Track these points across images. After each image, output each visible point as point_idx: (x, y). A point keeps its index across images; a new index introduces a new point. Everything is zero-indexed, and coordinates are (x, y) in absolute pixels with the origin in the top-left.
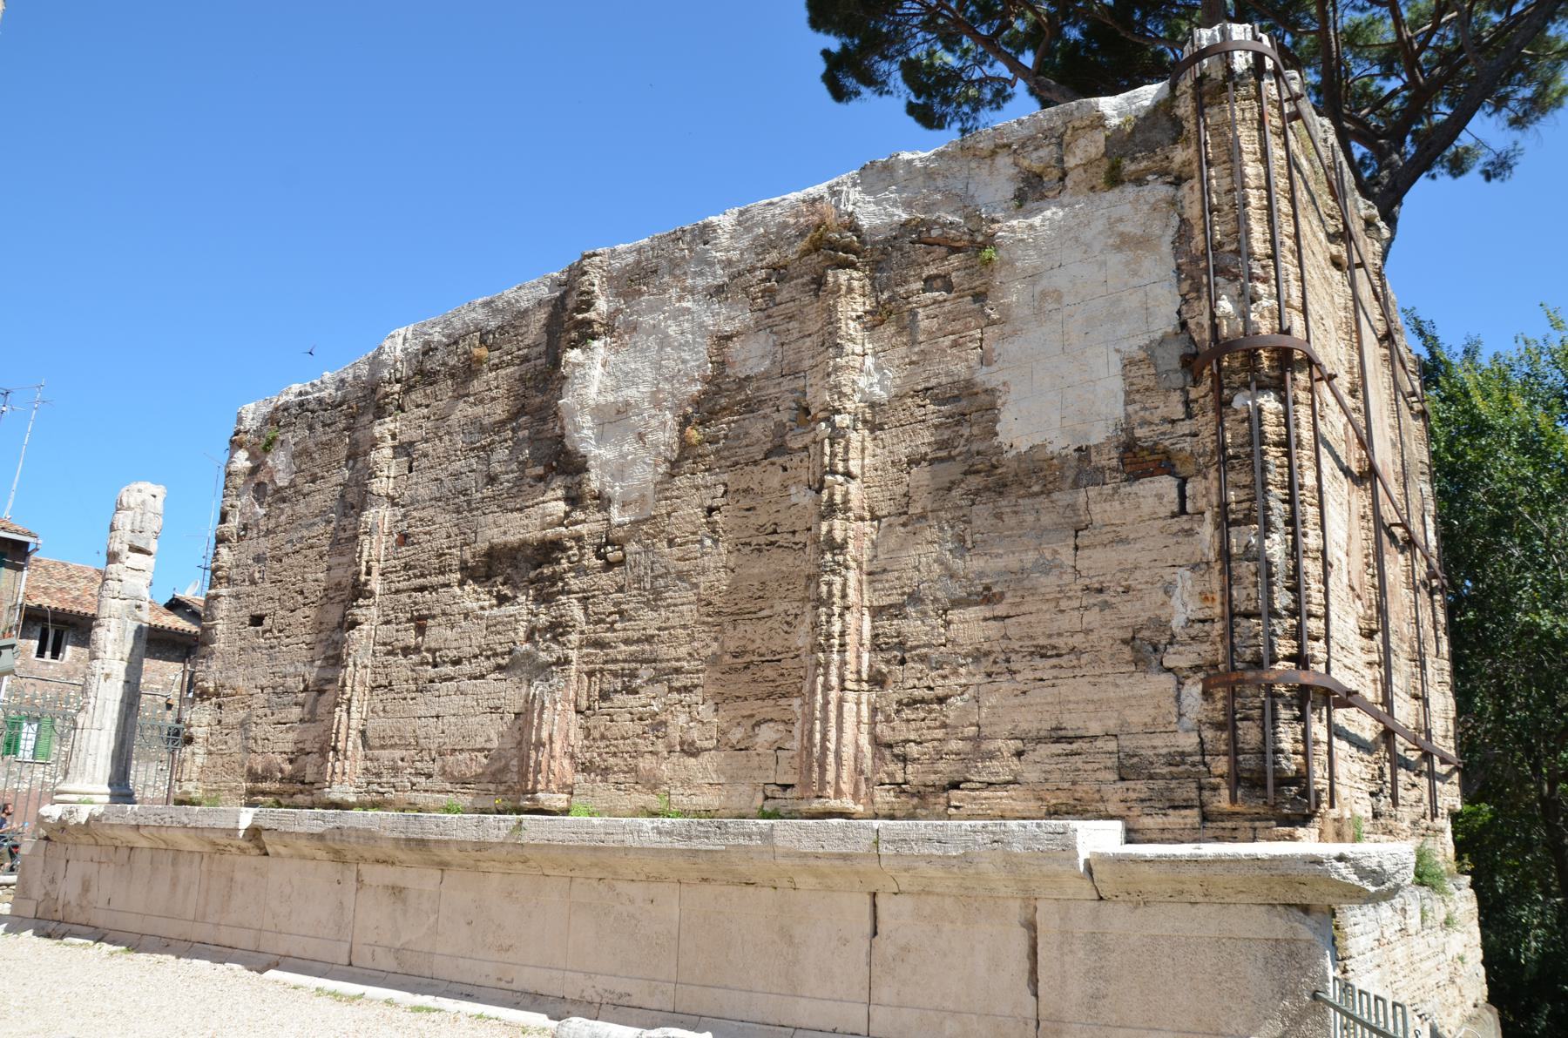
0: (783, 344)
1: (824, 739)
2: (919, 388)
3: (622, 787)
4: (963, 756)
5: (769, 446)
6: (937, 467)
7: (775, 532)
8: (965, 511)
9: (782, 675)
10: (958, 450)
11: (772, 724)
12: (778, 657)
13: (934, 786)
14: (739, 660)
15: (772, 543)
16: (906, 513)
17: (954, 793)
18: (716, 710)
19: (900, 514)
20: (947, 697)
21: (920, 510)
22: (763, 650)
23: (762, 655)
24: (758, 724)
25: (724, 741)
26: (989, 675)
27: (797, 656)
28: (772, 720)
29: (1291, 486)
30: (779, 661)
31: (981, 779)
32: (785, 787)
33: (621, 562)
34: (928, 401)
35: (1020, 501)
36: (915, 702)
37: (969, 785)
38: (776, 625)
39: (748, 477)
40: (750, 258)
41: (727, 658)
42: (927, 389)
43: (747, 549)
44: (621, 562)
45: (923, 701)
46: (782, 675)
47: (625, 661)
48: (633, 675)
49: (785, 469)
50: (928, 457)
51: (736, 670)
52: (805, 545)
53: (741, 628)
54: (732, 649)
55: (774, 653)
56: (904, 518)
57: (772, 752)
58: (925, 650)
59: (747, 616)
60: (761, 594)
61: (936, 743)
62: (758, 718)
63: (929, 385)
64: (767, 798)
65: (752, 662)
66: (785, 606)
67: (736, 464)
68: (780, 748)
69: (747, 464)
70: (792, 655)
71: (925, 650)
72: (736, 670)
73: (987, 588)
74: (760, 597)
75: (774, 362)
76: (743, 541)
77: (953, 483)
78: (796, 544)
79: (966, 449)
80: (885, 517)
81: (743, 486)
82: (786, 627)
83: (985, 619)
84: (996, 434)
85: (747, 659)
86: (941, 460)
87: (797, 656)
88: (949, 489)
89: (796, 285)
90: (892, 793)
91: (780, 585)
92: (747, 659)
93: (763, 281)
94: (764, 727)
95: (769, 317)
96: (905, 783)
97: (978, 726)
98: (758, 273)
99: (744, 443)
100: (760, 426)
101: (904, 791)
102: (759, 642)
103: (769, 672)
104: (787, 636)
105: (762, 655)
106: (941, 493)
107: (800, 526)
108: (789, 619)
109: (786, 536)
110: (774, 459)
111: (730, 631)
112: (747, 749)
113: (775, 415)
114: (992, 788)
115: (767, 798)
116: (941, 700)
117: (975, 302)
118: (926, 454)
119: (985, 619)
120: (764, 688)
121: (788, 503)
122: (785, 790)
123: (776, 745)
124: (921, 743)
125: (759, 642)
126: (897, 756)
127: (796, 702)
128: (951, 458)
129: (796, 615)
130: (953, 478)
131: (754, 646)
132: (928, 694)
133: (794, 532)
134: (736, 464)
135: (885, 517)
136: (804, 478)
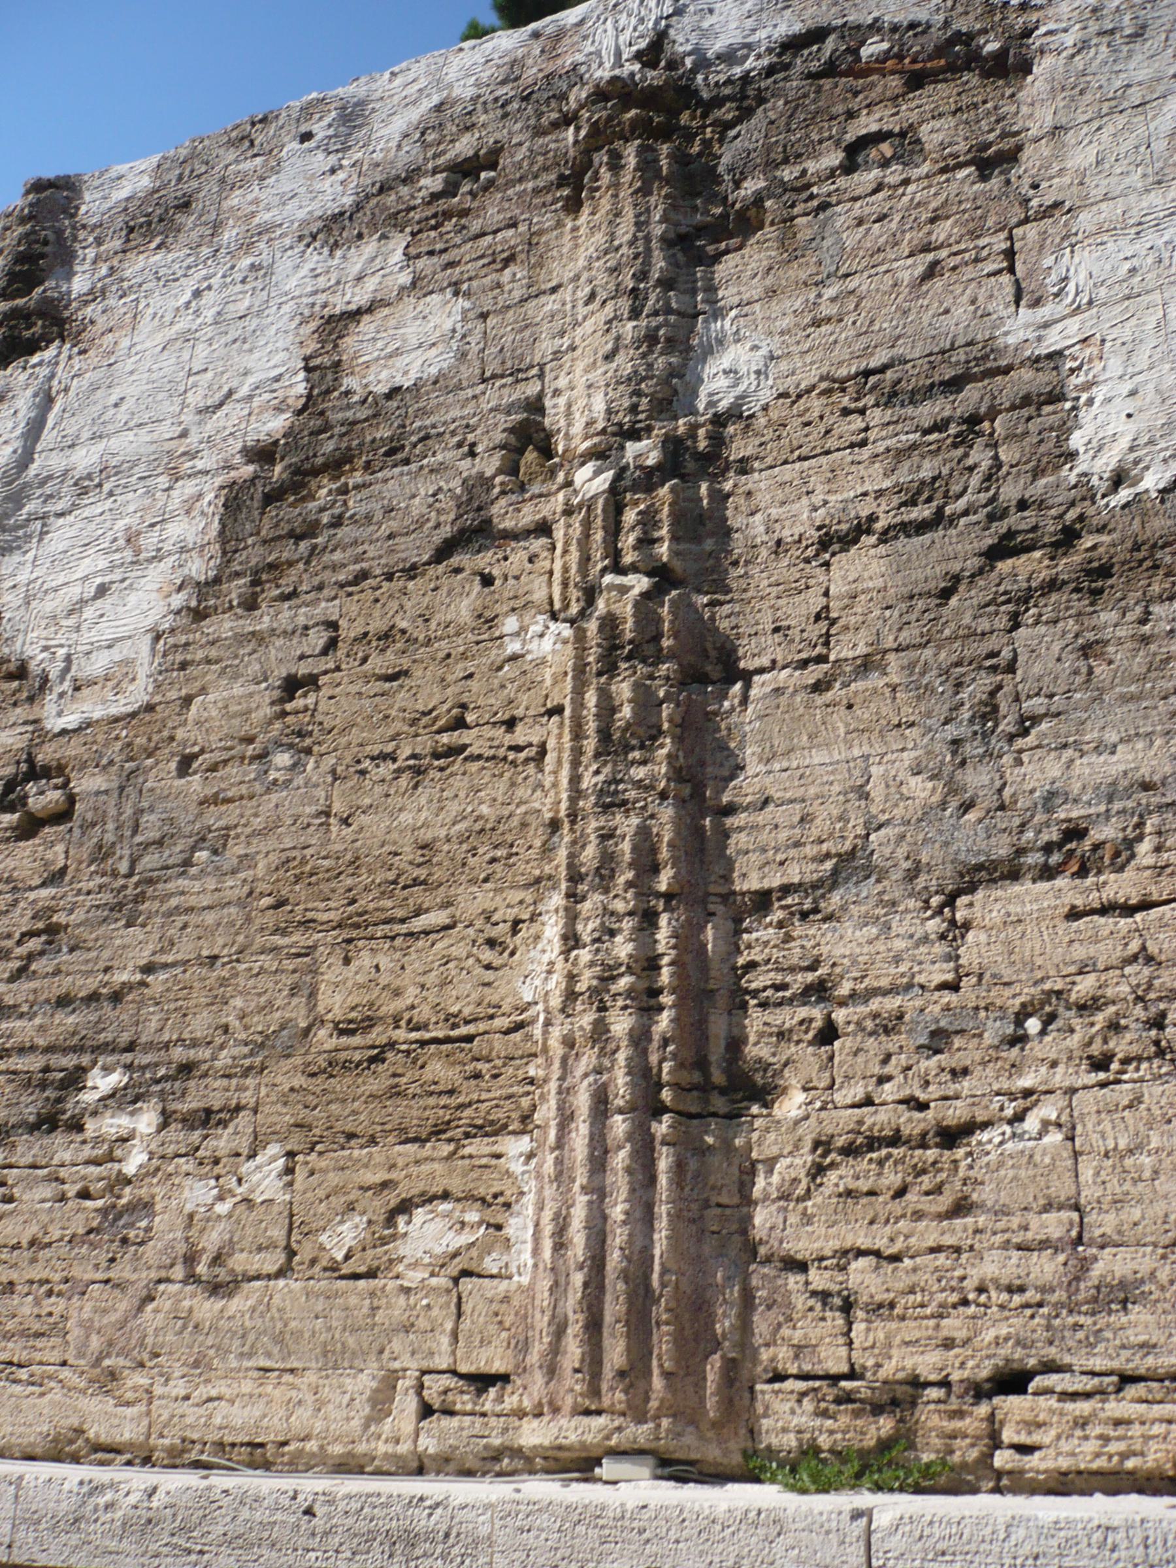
0: (484, 316)
1: (643, 1214)
2: (843, 372)
3: (23, 1374)
4: (1031, 1295)
5: (446, 531)
6: (902, 544)
7: (459, 724)
8: (992, 643)
9: (477, 1076)
10: (961, 504)
11: (445, 1207)
12: (464, 1030)
13: (945, 1383)
14: (356, 1040)
15: (454, 751)
16: (821, 659)
17: (1012, 1405)
18: (289, 1170)
19: (804, 664)
20: (969, 1128)
21: (862, 650)
22: (424, 1013)
23: (424, 1026)
24: (405, 1207)
25: (305, 1252)
26: (1100, 1064)
27: (519, 1026)
28: (445, 1196)
29: (599, 1193)
30: (469, 1039)
31: (1098, 1364)
32: (482, 1381)
33: (62, 816)
34: (869, 400)
35: (1156, 609)
36: (873, 1143)
37: (1051, 1380)
38: (460, 951)
39: (394, 605)
40: (411, 153)
41: (324, 1038)
42: (867, 373)
43: (386, 769)
44: (62, 816)
45: (895, 1140)
46: (477, 1076)
47: (50, 1049)
48: (75, 1080)
49: (487, 581)
50: (879, 526)
51: (346, 1066)
52: (543, 751)
53: (365, 960)
54: (337, 1013)
55: (452, 1020)
56: (814, 673)
57: (442, 1281)
58: (891, 1004)
59: (380, 931)
60: (422, 873)
61: (942, 1259)
62: (405, 1190)
63: (874, 363)
64: (426, 1411)
65: (392, 1045)
66: (484, 898)
67: (363, 575)
68: (466, 1273)
69: (389, 577)
70: (501, 1023)
71: (891, 1004)
72: (346, 1066)
73: (1075, 833)
74: (416, 882)
75: (463, 356)
76: (376, 750)
77: (956, 579)
78: (518, 749)
79: (984, 497)
80: (761, 671)
81: (378, 625)
82: (487, 955)
83: (1074, 914)
84: (1072, 456)
85: (378, 1035)
86: (921, 527)
87: (519, 1026)
88: (946, 594)
89: (520, 195)
90: (808, 1405)
91: (473, 851)
92: (378, 1035)
93: (435, 197)
94: (420, 1214)
95: (451, 265)
96: (852, 1375)
97: (1077, 1208)
98: (424, 182)
99: (384, 530)
100: (425, 488)
101: (846, 1398)
102: (411, 994)
103: (438, 1070)
104: (489, 976)
105: (424, 1026)
106: (920, 604)
107: (527, 704)
108: (494, 932)
109: (488, 731)
110: (455, 561)
111: (332, 971)
112: (371, 1274)
113: (465, 464)
114: (1132, 1391)
115: (426, 1411)
116: (950, 1136)
117: (984, 178)
118: (873, 518)
119: (1074, 914)
120: (433, 1110)
121: (495, 655)
122: (481, 1392)
123: (454, 1269)
124: (896, 1258)
125: (412, 991)
126: (824, 1296)
127: (515, 1146)
128: (938, 520)
129: (516, 923)
130: (956, 567)
131: (399, 1004)
132: (912, 1123)
133: (510, 724)
134: (363, 575)
135: (761, 671)
136: (539, 595)
